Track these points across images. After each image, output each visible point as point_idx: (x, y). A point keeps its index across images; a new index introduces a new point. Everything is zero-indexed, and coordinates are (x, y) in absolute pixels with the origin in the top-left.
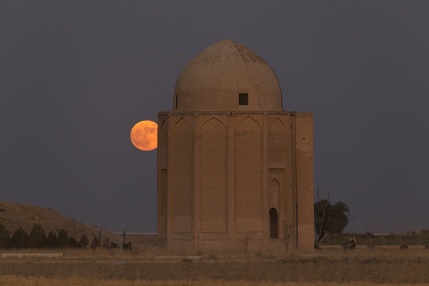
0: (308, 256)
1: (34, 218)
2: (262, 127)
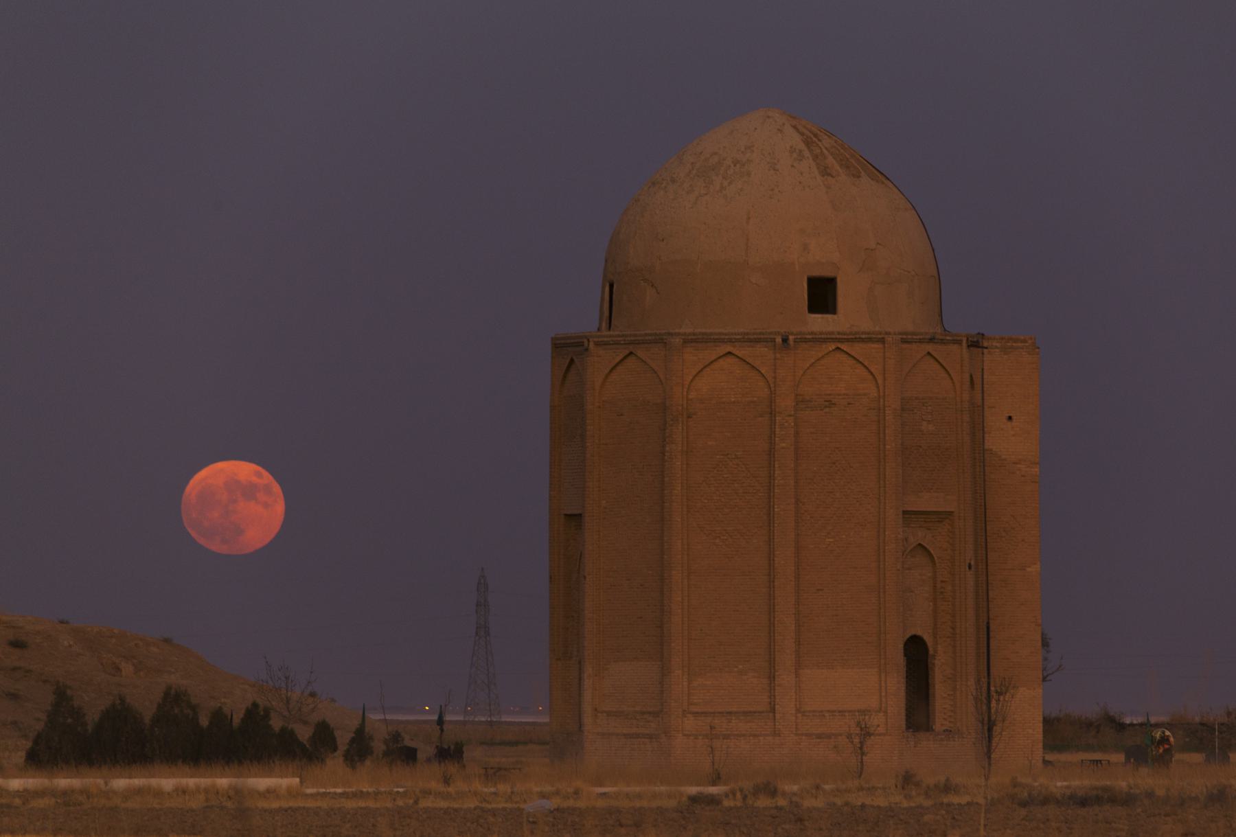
0: (1059, 784)
1: (118, 669)
2: (880, 381)
